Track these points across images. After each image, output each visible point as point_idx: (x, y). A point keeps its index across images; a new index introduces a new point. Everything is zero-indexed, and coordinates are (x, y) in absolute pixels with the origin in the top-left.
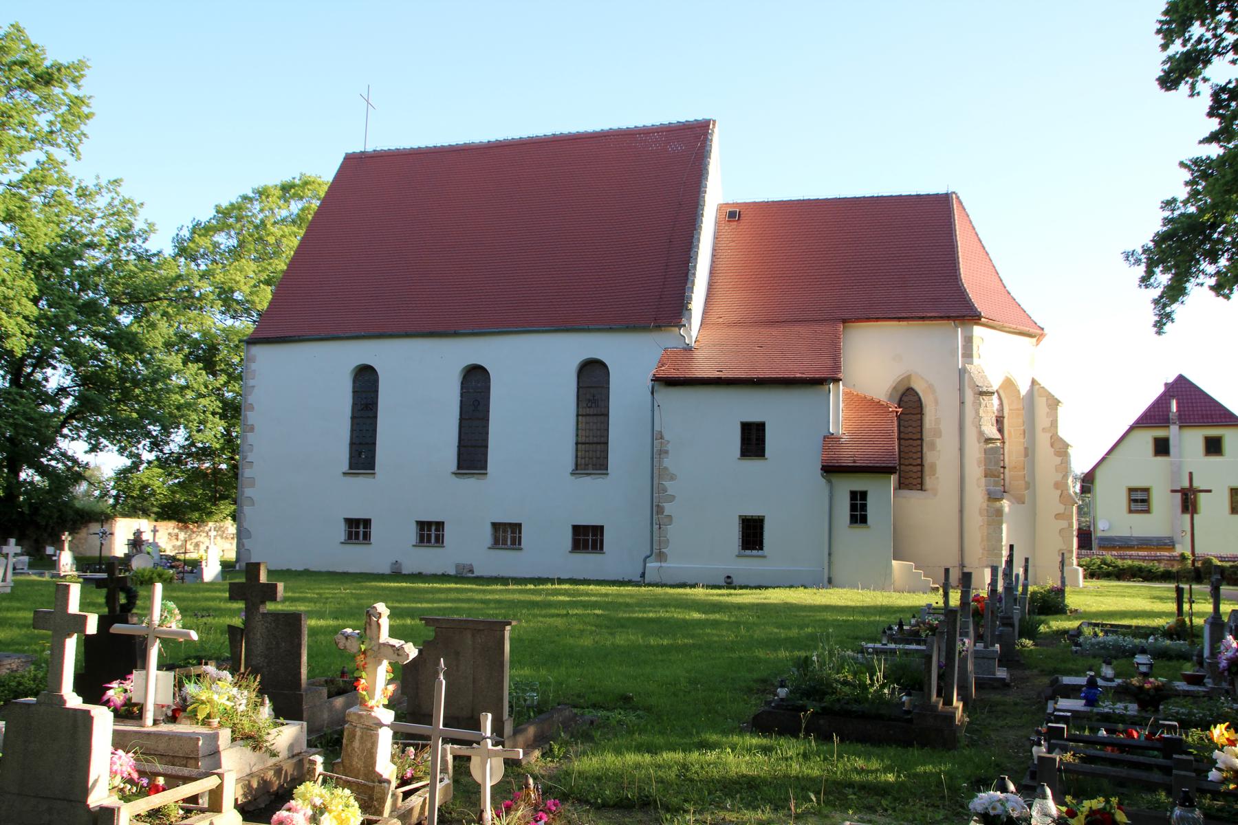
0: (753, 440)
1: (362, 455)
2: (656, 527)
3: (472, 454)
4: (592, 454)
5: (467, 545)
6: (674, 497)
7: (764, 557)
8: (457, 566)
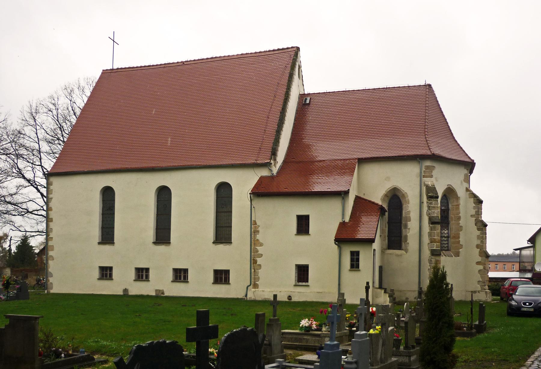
0: (303, 225)
1: (107, 236)
2: (253, 270)
3: (163, 235)
4: (223, 234)
5: (161, 283)
6: (262, 255)
7: (308, 286)
8: (156, 291)
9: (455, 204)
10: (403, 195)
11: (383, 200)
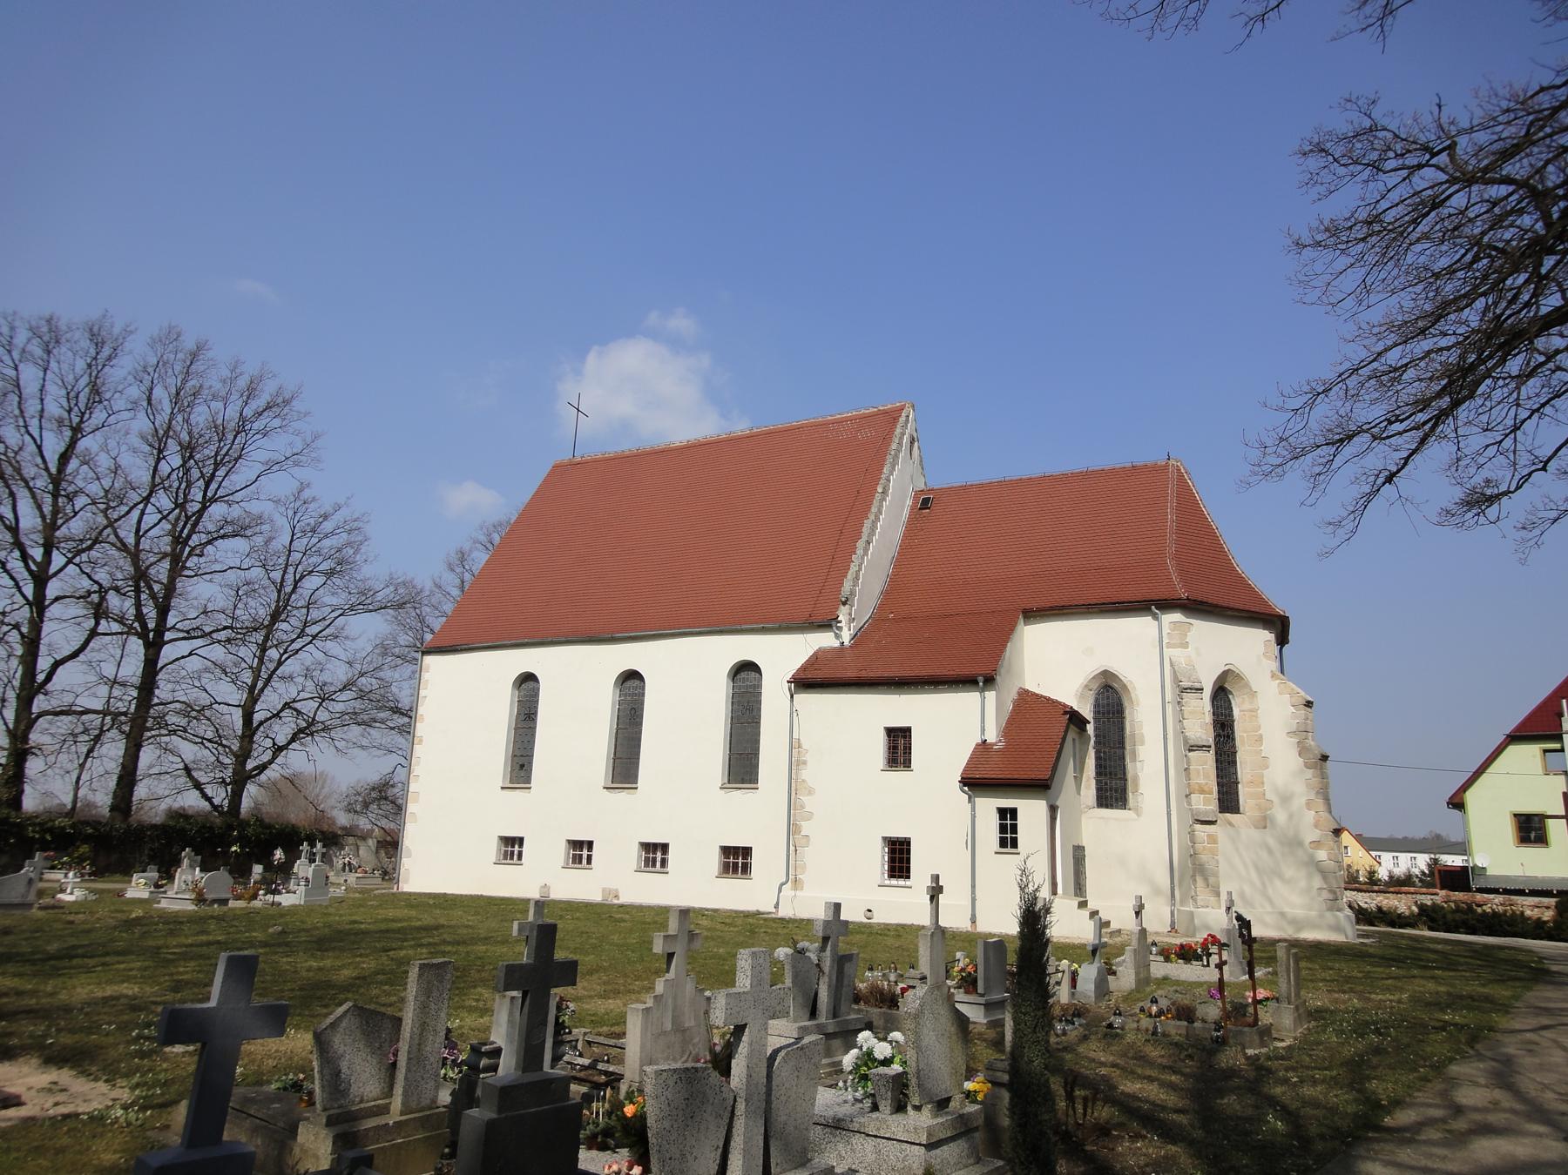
0: (899, 745)
1: (520, 768)
3: (624, 766)
4: (742, 766)
8: (604, 890)
9: (1247, 706)
10: (1125, 686)
11: (1082, 697)
